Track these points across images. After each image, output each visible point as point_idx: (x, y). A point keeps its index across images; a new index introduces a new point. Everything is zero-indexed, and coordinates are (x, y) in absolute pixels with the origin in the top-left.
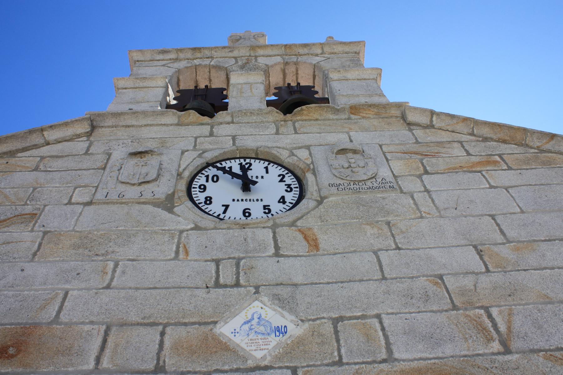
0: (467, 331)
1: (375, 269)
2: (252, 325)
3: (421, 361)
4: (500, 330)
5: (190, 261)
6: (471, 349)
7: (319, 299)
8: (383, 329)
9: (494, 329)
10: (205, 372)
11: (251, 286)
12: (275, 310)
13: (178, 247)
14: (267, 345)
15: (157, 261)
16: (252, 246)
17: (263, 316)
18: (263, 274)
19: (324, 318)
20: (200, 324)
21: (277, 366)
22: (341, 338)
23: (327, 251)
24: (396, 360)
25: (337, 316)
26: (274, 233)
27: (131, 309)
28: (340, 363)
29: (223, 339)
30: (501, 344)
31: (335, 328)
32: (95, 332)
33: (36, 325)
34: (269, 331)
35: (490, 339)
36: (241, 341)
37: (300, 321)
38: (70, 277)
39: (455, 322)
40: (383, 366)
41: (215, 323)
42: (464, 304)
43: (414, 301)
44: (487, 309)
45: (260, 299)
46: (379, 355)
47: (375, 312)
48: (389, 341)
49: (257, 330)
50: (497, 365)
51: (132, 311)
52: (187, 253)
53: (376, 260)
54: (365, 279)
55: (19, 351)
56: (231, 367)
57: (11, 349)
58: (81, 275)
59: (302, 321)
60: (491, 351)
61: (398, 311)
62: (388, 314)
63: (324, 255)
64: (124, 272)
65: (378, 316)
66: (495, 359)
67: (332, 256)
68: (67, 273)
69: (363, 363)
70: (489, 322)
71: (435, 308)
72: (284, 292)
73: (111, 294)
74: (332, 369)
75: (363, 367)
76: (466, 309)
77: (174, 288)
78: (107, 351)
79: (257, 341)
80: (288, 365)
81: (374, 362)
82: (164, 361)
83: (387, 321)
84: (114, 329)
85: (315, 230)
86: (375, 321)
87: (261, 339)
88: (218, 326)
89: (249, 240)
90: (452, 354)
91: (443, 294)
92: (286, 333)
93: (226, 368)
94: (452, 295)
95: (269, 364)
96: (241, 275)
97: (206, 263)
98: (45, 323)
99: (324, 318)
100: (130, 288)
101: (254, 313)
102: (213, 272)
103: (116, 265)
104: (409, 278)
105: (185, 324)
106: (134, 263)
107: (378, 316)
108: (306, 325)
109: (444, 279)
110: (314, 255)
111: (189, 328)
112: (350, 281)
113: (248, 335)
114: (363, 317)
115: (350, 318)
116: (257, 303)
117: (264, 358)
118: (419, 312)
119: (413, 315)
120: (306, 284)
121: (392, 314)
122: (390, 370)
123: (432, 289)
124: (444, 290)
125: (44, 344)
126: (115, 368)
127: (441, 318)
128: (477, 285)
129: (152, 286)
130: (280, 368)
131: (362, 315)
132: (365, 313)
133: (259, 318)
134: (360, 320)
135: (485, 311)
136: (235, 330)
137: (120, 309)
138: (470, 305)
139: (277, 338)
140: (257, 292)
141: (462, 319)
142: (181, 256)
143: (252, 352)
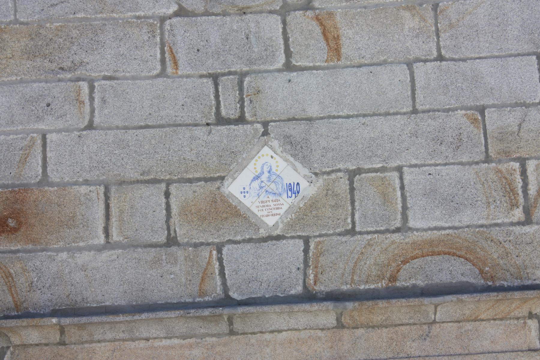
0: (493, 192)
1: (406, 94)
2: (262, 182)
3: (435, 232)
4: (529, 192)
5: (181, 77)
6: (491, 217)
7: (336, 141)
8: (402, 188)
9: (523, 192)
10: (218, 243)
11: (258, 122)
12: (286, 160)
13: (163, 53)
14: (278, 208)
15: (141, 79)
16: (256, 50)
17: (274, 170)
18: (272, 102)
19: (339, 170)
20: (206, 180)
21: (289, 235)
22: (356, 198)
23: (351, 60)
24: (410, 229)
25: (354, 167)
26: (284, 22)
27: (125, 160)
28: (352, 232)
29: (233, 201)
30: (524, 212)
31: (351, 183)
32: (94, 195)
33: (26, 188)
34: (280, 190)
35: (514, 205)
36: (251, 202)
37: (313, 176)
38: (40, 111)
39: (483, 179)
40: (396, 237)
41: (222, 178)
42: (499, 153)
43: (443, 148)
44: (523, 162)
45: (270, 143)
46: (393, 222)
47: (397, 163)
48: (406, 203)
49: (268, 189)
50: (511, 238)
51: (127, 163)
52: (175, 63)
53: (409, 79)
54: (392, 111)
55: (20, 224)
56: (243, 238)
57: (10, 220)
58: (52, 106)
59: (316, 174)
60: (511, 220)
61: (423, 162)
62: (411, 166)
63: (347, 67)
64: (104, 101)
65: (399, 169)
66: (512, 231)
67: (355, 69)
68: (34, 104)
69: (376, 232)
70: (520, 180)
71: (465, 159)
72: (296, 130)
73: (97, 137)
74: (344, 239)
75: (375, 238)
76: (500, 161)
77: (169, 126)
78: (114, 220)
79: (268, 203)
80: (300, 234)
81: (387, 231)
82: (175, 231)
83: (408, 178)
84: (113, 189)
85: (338, 18)
86: (396, 174)
87: (272, 201)
88: (226, 183)
89: (253, 39)
90: (468, 223)
91: (479, 138)
92: (298, 193)
93: (239, 238)
94: (489, 141)
95: (281, 234)
96: (246, 104)
97: (201, 80)
98: (34, 184)
99: (339, 170)
100: (118, 128)
101: (264, 164)
102: (212, 97)
103: (92, 88)
104: (445, 111)
105: (190, 181)
106: (113, 83)
107: (399, 169)
108: (321, 181)
109: (486, 114)
110: (334, 68)
111: (196, 186)
112: (374, 115)
113: (259, 196)
114: (383, 170)
115: (370, 171)
116: (266, 150)
117: (276, 225)
118: (445, 164)
119: (438, 168)
120: (322, 118)
121: (415, 166)
122: (402, 241)
123: (469, 128)
124: (482, 131)
125: (43, 213)
126: (126, 240)
127: (469, 173)
128: (523, 125)
129: (142, 124)
130: (293, 237)
131: (383, 167)
132: (386, 165)
133: (269, 172)
134: (378, 173)
135: (520, 164)
136: (244, 188)
137: (114, 160)
138: (507, 155)
139: (290, 200)
140: (266, 133)
141: (492, 176)
142: (170, 70)
143: (263, 219)
